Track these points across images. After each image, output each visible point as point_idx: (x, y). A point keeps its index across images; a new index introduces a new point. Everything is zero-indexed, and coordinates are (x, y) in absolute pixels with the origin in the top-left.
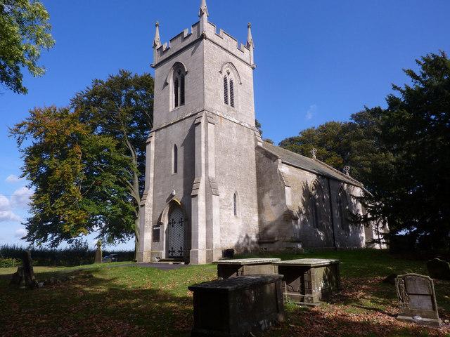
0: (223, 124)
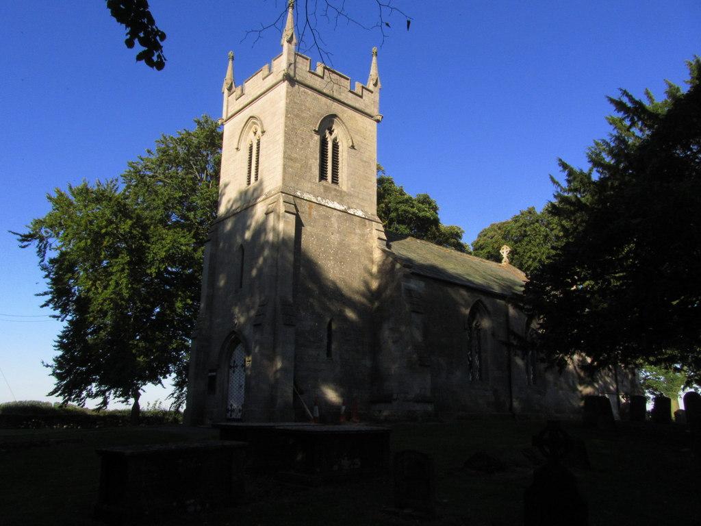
0: (314, 213)
